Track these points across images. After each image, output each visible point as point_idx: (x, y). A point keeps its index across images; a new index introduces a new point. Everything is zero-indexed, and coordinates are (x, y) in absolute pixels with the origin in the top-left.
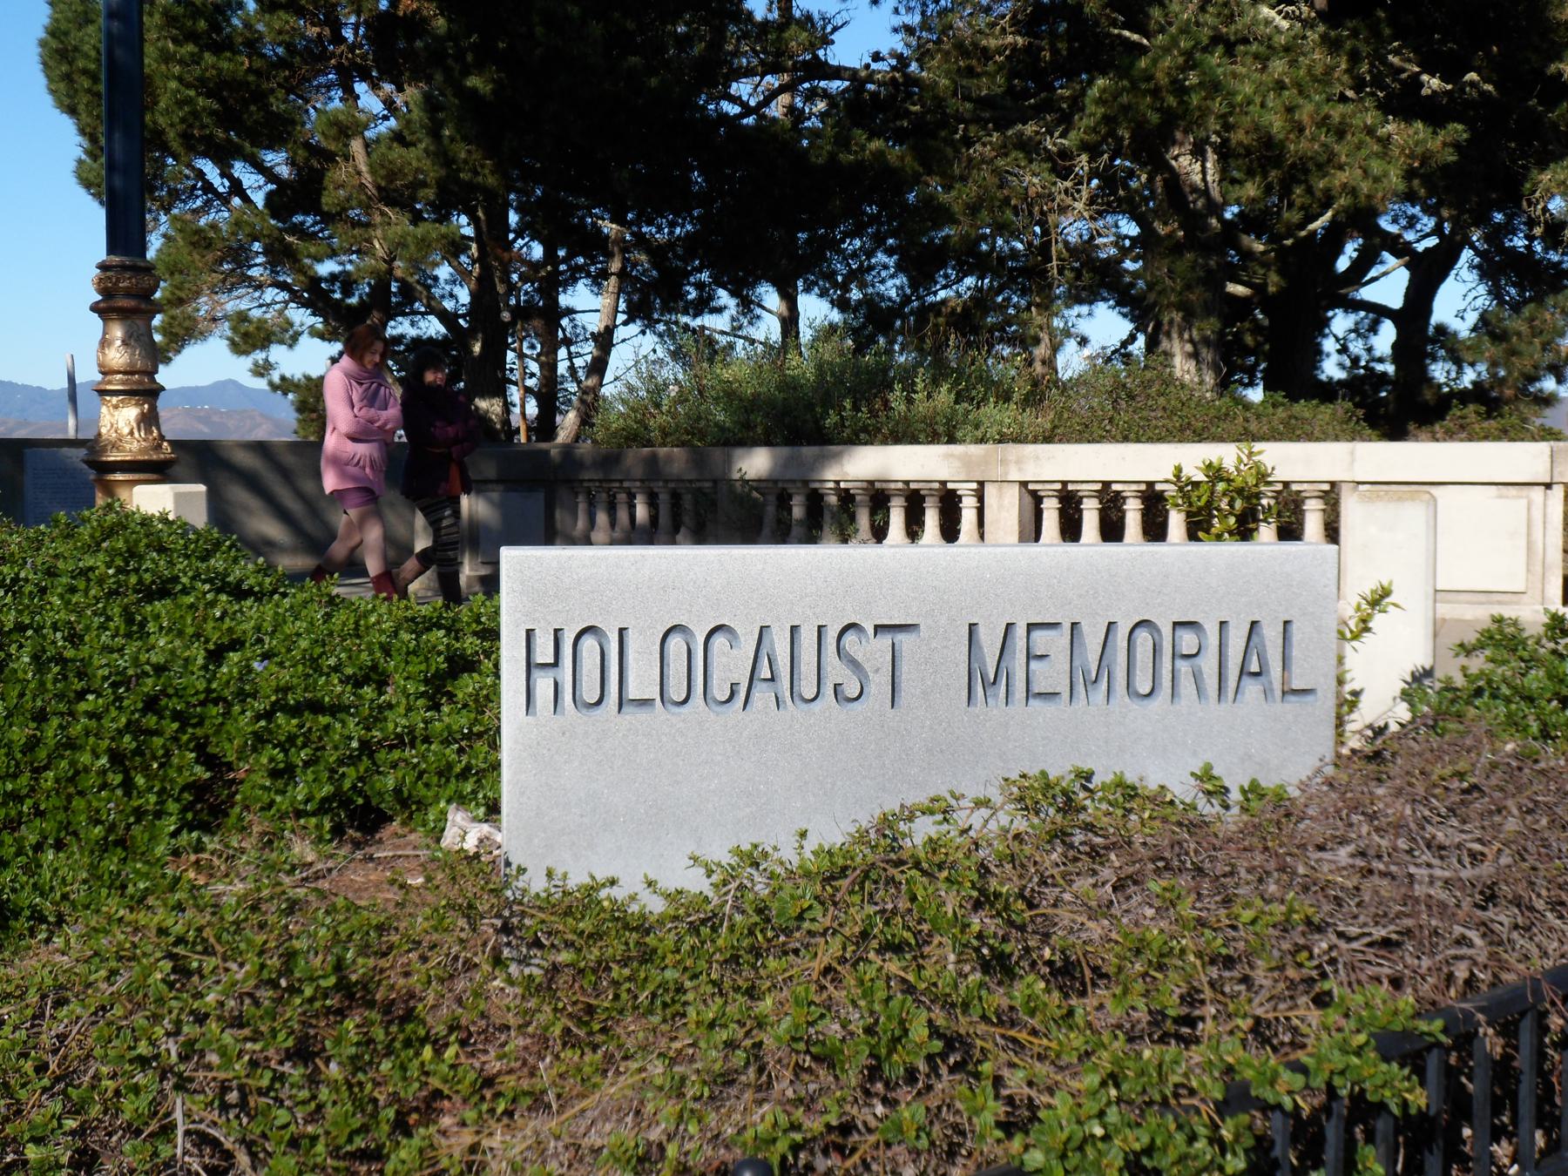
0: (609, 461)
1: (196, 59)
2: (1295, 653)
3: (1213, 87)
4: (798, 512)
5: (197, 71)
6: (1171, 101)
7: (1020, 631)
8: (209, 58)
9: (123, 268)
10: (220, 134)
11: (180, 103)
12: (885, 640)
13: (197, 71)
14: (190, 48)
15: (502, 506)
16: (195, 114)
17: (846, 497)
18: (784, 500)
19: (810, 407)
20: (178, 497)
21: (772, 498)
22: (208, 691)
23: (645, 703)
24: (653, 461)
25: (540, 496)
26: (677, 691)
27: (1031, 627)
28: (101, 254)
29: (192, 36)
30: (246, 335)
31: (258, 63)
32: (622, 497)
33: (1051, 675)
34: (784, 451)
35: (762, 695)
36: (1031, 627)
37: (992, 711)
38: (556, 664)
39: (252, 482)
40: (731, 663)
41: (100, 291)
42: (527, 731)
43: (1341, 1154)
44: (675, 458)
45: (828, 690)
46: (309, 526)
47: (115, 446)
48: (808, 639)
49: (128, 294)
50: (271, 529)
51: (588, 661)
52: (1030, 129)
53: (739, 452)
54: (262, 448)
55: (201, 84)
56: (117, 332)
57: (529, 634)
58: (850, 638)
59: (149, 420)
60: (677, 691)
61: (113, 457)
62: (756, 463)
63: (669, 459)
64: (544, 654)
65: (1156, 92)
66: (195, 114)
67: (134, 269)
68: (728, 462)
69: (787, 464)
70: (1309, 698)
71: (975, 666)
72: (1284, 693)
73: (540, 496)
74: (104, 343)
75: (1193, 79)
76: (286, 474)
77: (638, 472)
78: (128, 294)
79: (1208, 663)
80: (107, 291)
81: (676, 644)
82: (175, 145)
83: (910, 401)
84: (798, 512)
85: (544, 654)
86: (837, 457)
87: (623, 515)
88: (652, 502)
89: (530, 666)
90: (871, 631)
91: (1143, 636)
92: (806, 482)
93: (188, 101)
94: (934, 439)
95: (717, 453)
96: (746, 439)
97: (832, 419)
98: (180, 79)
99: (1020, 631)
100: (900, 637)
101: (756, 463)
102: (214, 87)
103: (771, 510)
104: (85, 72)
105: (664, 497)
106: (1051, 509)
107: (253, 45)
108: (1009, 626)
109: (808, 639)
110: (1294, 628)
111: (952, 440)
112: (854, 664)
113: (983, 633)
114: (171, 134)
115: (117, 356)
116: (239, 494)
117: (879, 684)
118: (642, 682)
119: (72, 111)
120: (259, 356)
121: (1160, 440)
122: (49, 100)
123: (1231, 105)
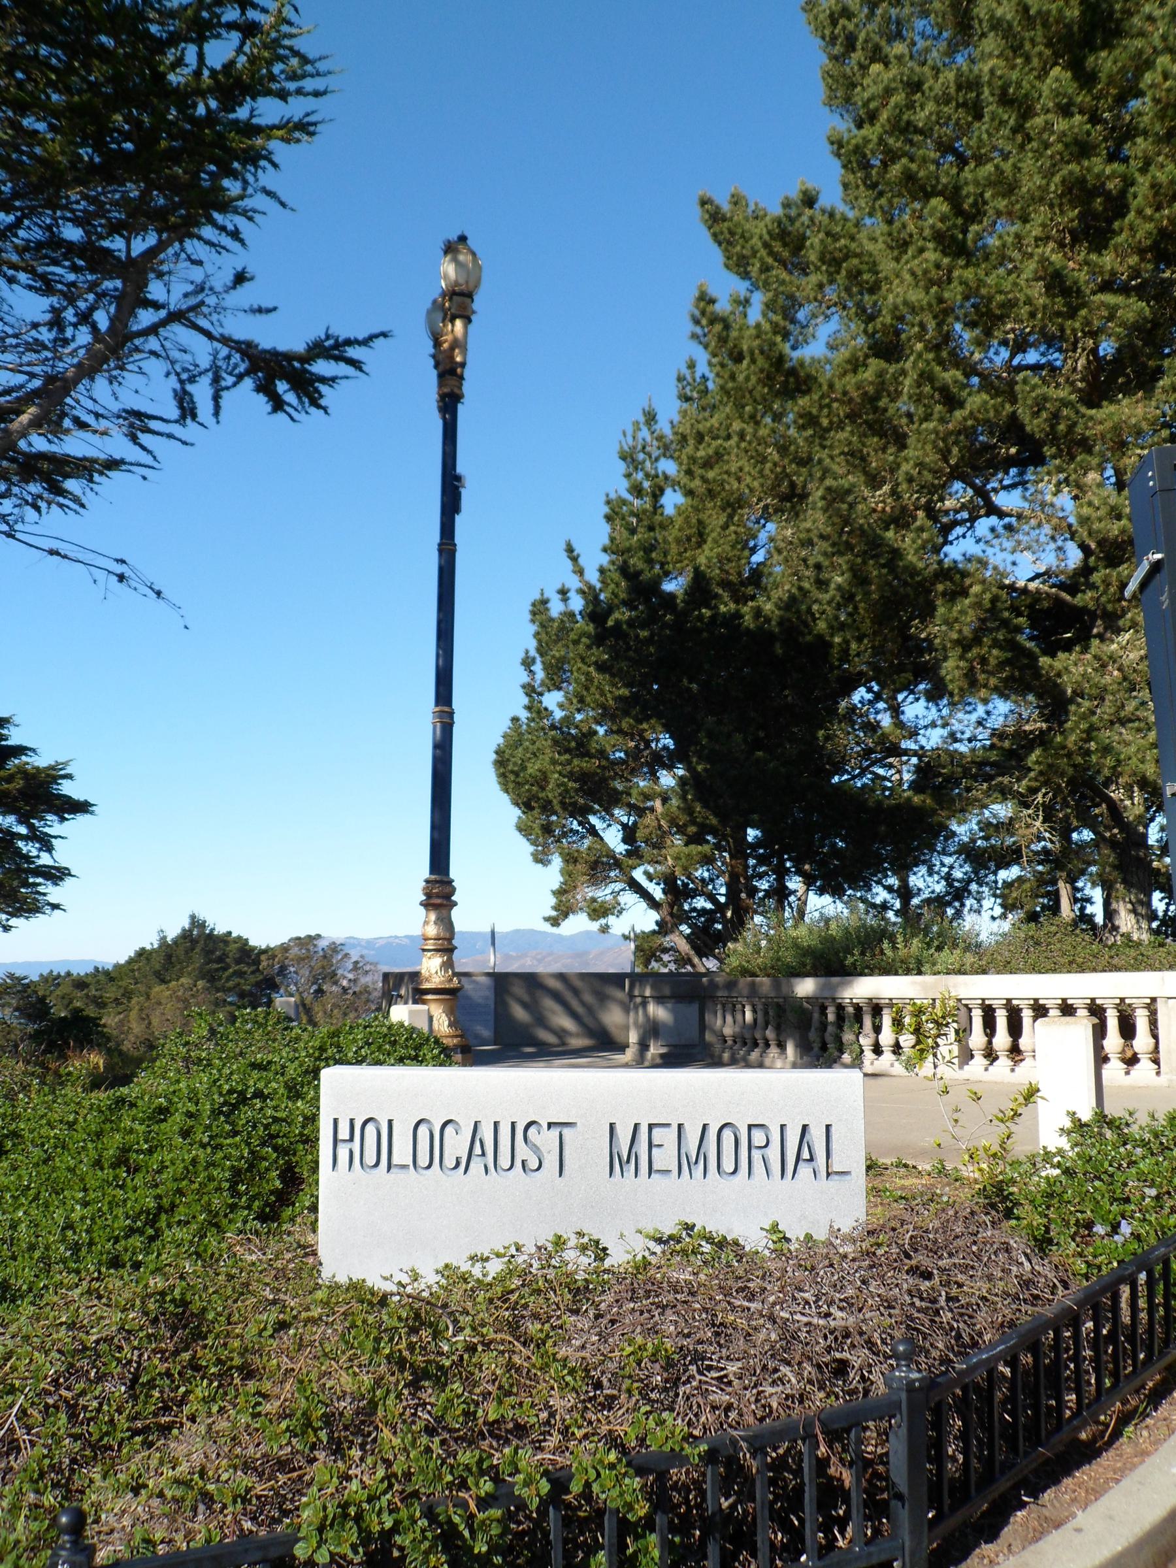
0: (731, 985)
1: (569, 762)
2: (834, 1146)
3: (1106, 750)
4: (831, 1017)
5: (568, 768)
6: (1079, 760)
7: (644, 1129)
8: (576, 762)
9: (436, 882)
10: (582, 801)
11: (558, 786)
12: (555, 1132)
13: (568, 768)
14: (567, 756)
15: (673, 1011)
16: (567, 791)
17: (858, 1008)
18: (823, 1009)
19: (837, 954)
20: (411, 1012)
21: (817, 1009)
22: (301, 1134)
23: (404, 1167)
24: (753, 984)
25: (695, 1007)
26: (423, 1160)
27: (651, 1127)
28: (426, 874)
29: (568, 750)
30: (594, 910)
31: (604, 763)
32: (739, 1007)
33: (666, 1157)
34: (822, 980)
35: (477, 1165)
36: (651, 1127)
37: (627, 1182)
38: (351, 1139)
39: (557, 996)
40: (456, 1145)
41: (426, 894)
42: (335, 1185)
43: (615, 1541)
44: (764, 982)
45: (518, 1163)
46: (587, 1020)
47: (427, 980)
48: (505, 1132)
49: (438, 896)
50: (567, 1023)
51: (374, 1142)
52: (1006, 780)
53: (798, 980)
54: (562, 977)
55: (571, 776)
56: (433, 917)
57: (336, 1121)
58: (532, 1131)
59: (448, 964)
60: (423, 1160)
61: (426, 986)
62: (806, 987)
63: (761, 984)
64: (344, 1134)
65: (1069, 755)
66: (567, 791)
67: (441, 882)
68: (791, 987)
69: (822, 988)
70: (848, 1177)
71: (615, 1151)
72: (828, 1174)
73: (695, 1007)
74: (426, 923)
75: (1093, 745)
76: (576, 992)
77: (745, 992)
78: (438, 896)
79: (774, 1153)
80: (429, 895)
81: (423, 1131)
82: (557, 807)
83: (894, 948)
84: (831, 1017)
85: (344, 1134)
86: (850, 983)
87: (739, 1017)
88: (754, 1011)
89: (336, 1141)
90: (545, 1126)
91: (728, 1135)
92: (834, 999)
93: (563, 784)
94: (908, 972)
95: (784, 980)
96: (800, 973)
97: (850, 960)
98: (560, 773)
99: (644, 1129)
100: (566, 1131)
101: (806, 987)
102: (583, 777)
103: (816, 1016)
104: (512, 772)
105: (759, 1007)
106: (977, 1015)
107: (602, 754)
108: (636, 1126)
109: (505, 1132)
110: (833, 1130)
111: (920, 973)
112: (536, 1149)
113: (619, 1129)
114: (555, 802)
115: (432, 930)
116: (549, 1003)
117: (551, 1161)
118: (402, 1154)
119: (507, 791)
120: (603, 921)
121: (1047, 972)
122: (498, 787)
123: (1119, 761)
